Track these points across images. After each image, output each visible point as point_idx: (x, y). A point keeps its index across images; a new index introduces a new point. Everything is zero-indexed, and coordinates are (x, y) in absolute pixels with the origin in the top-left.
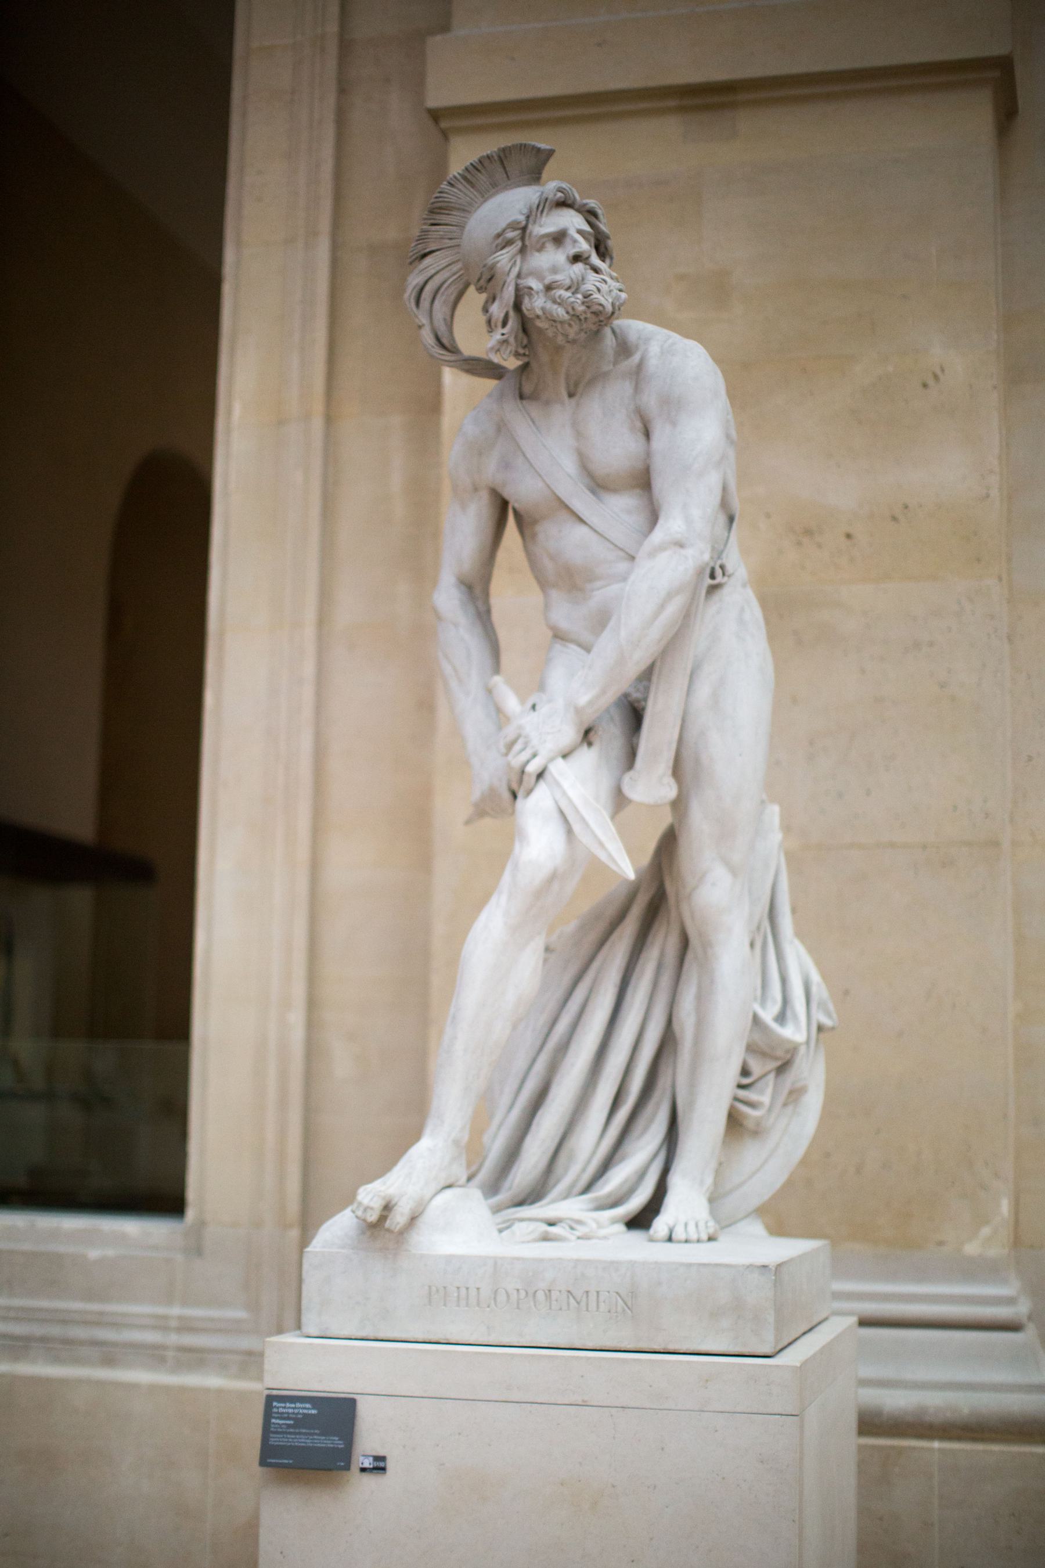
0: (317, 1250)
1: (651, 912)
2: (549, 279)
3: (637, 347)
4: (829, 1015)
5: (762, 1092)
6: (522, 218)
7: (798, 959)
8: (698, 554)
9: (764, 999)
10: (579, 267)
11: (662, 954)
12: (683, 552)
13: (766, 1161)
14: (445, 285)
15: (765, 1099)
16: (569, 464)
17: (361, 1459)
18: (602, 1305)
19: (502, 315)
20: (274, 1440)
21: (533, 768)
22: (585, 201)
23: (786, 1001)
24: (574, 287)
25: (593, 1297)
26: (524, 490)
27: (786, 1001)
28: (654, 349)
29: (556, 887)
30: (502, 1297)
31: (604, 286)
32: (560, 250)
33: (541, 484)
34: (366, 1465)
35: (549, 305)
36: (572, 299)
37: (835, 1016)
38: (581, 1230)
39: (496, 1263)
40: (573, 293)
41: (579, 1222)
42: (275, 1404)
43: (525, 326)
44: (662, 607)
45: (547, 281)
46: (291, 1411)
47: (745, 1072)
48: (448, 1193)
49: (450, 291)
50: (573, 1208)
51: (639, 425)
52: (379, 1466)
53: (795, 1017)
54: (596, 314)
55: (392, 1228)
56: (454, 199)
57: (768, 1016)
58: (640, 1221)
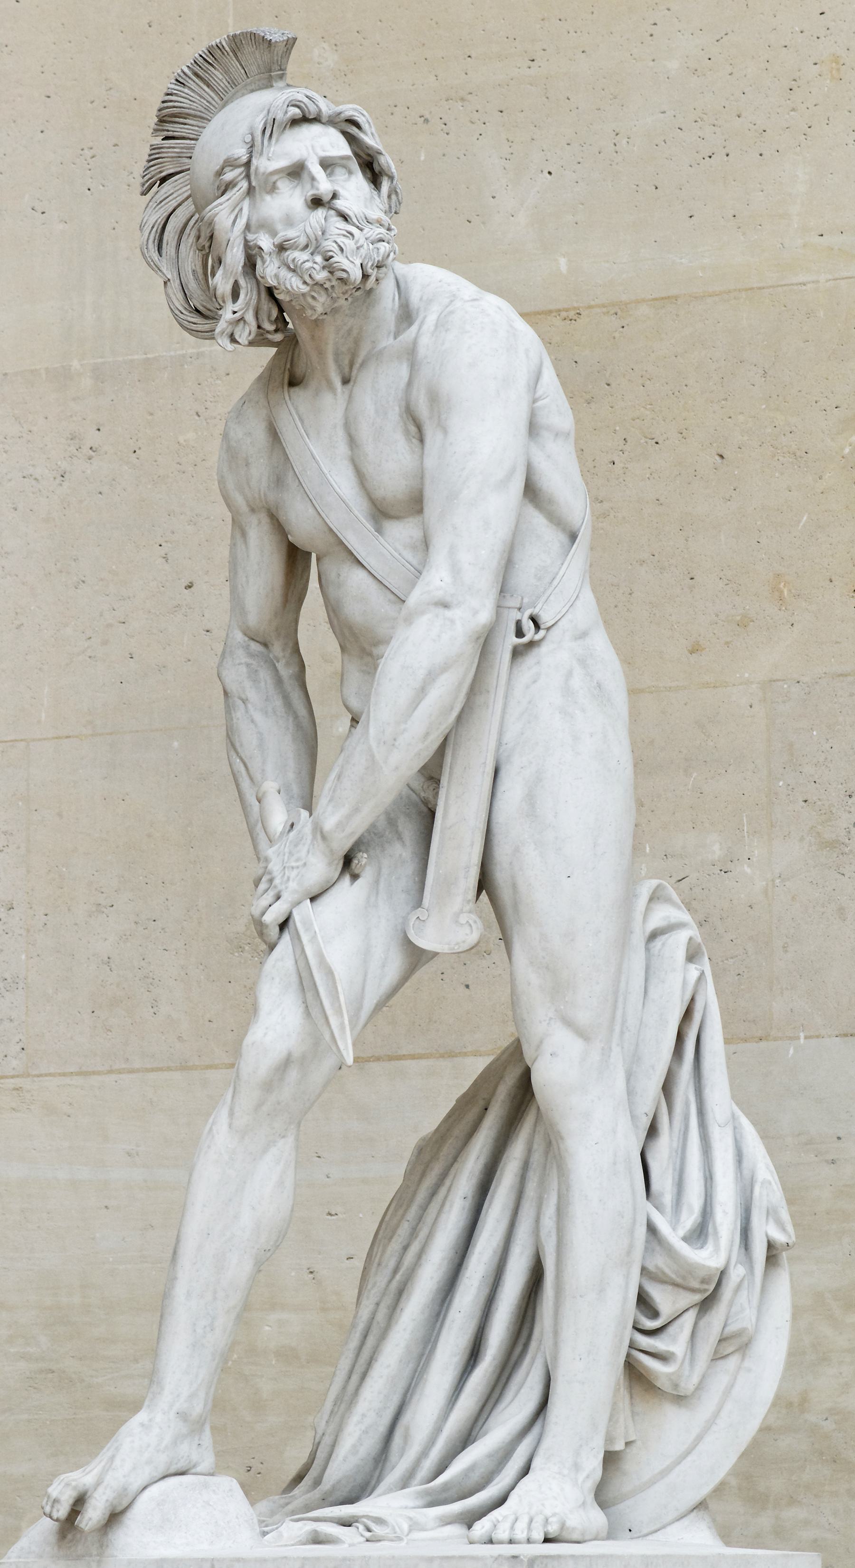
0: (11, 1560)
4: (783, 1229)
5: (674, 1340)
6: (241, 153)
11: (529, 1151)
12: (448, 613)
13: (699, 1438)
16: (344, 483)
19: (228, 288)
21: (272, 917)
22: (339, 109)
23: (707, 1213)
24: (313, 246)
27: (707, 1213)
29: (293, 1074)
33: (311, 510)
35: (284, 273)
36: (308, 265)
37: (790, 1228)
40: (312, 254)
44: (422, 691)
51: (413, 429)
56: (186, 103)
57: (673, 1235)
58: (470, 1519)
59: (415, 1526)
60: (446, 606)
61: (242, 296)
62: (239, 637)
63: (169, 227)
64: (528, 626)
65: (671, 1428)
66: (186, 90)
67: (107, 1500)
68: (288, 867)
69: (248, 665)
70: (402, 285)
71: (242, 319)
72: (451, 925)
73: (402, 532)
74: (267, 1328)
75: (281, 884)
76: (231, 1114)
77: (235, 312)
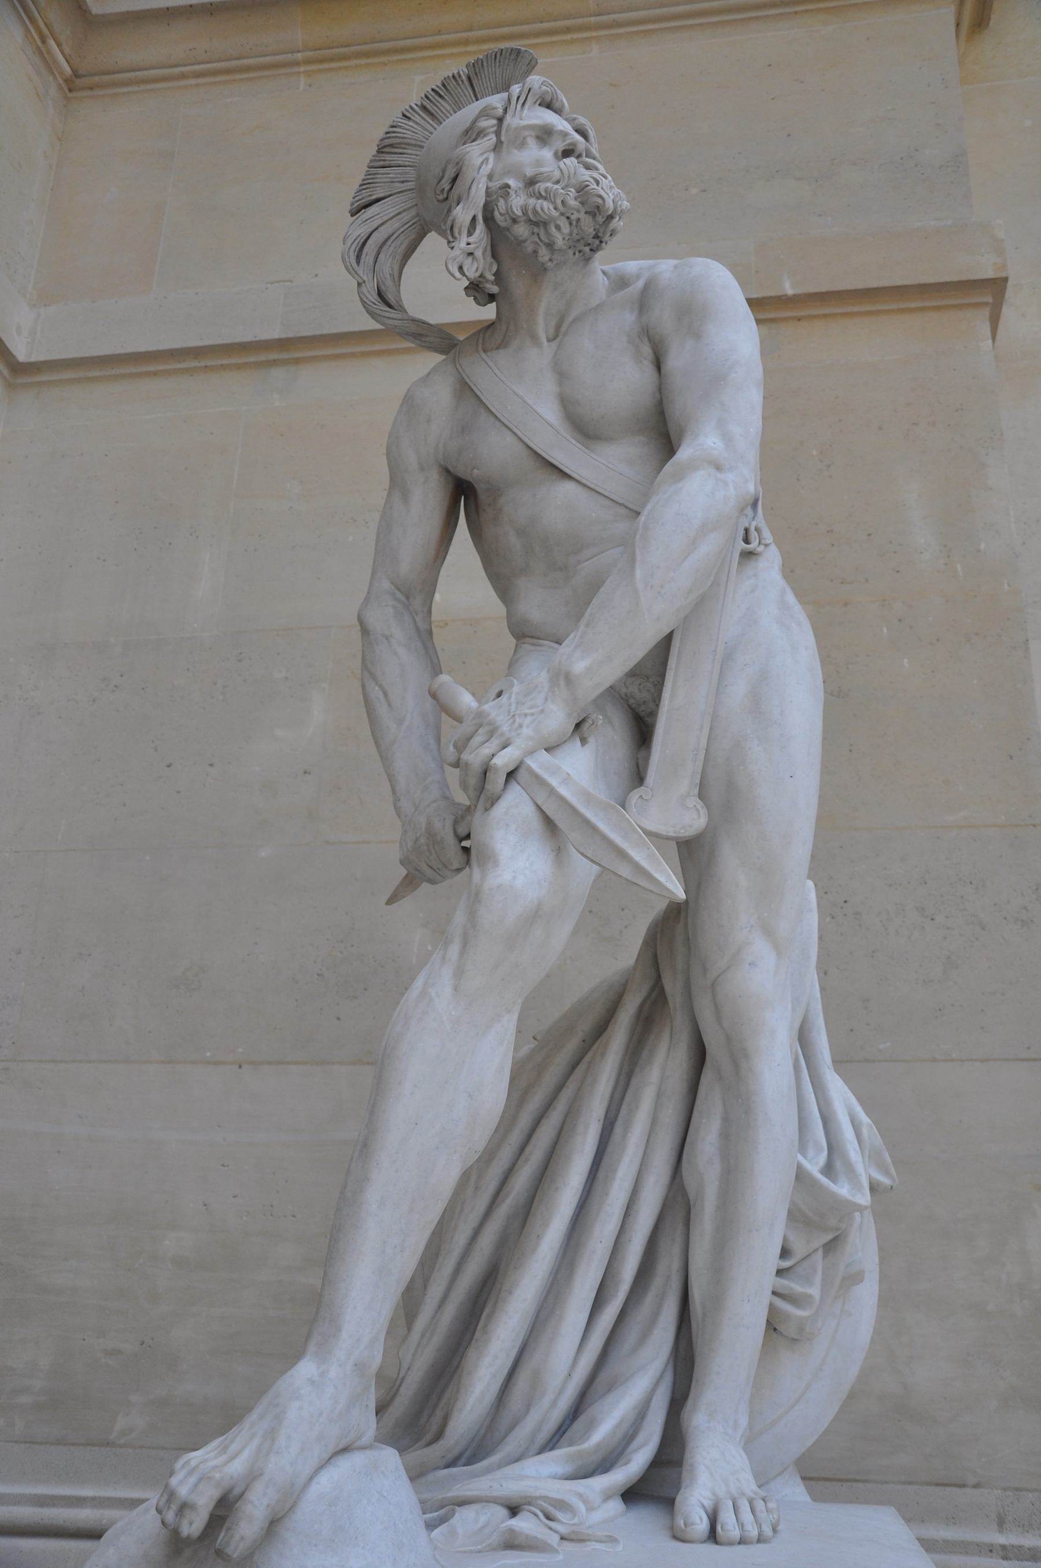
1: (653, 1005)
2: (529, 172)
4: (887, 1173)
5: (808, 1281)
7: (841, 1094)
9: (803, 1148)
10: (571, 161)
12: (719, 475)
14: (389, 243)
15: (815, 1291)
16: (550, 411)
21: (503, 760)
26: (493, 454)
33: (510, 438)
35: (532, 201)
37: (893, 1171)
38: (565, 1523)
41: (562, 1505)
47: (785, 1253)
48: (345, 1465)
49: (399, 241)
50: (540, 1475)
51: (647, 350)
55: (229, 1550)
57: (814, 1166)
62: (386, 585)
63: (370, 241)
66: (411, 123)
67: (268, 1506)
68: (519, 715)
69: (394, 607)
74: (167, 1242)
75: (510, 731)
76: (459, 973)
77: (468, 244)
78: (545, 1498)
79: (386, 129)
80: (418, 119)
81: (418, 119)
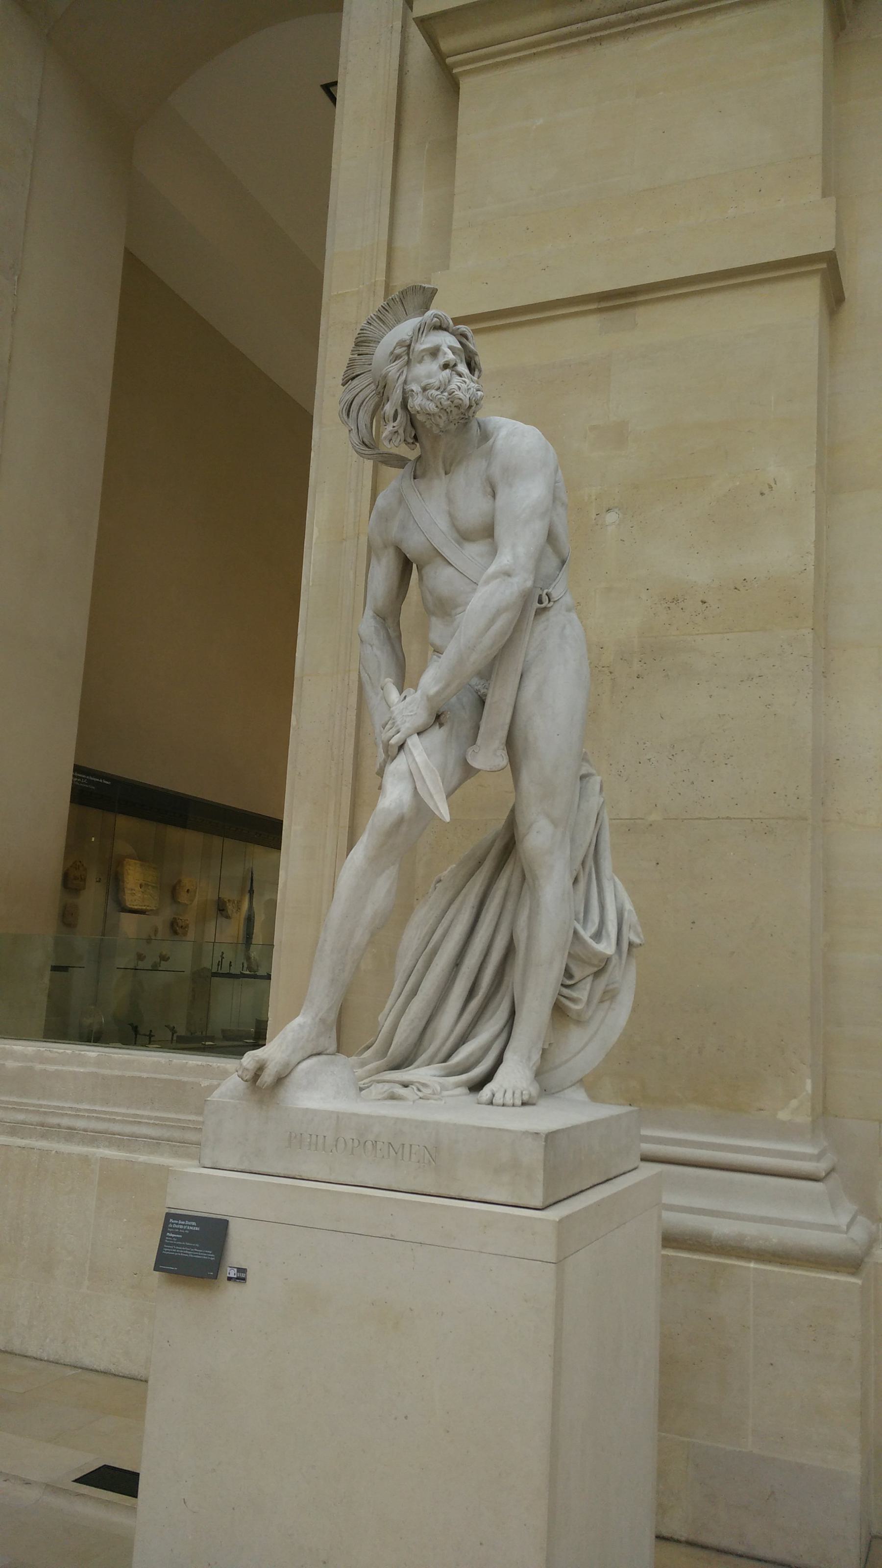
3: (493, 434)
4: (639, 937)
8: (522, 581)
12: (510, 579)
16: (443, 523)
17: (229, 1269)
18: (413, 1156)
19: (393, 412)
20: (166, 1251)
25: (407, 1149)
26: (413, 545)
28: (503, 433)
30: (341, 1145)
31: (463, 386)
32: (435, 362)
34: (232, 1275)
37: (642, 936)
39: (338, 1117)
41: (425, 1085)
42: (171, 1220)
43: (412, 421)
45: (423, 384)
46: (181, 1227)
48: (314, 1060)
51: (489, 490)
52: (241, 1277)
53: (608, 935)
54: (458, 407)
56: (371, 334)
57: (586, 935)
58: (477, 1086)
59: (444, 1088)
60: (509, 575)
61: (399, 419)
64: (545, 599)
65: (576, 1037)
70: (482, 425)
71: (396, 432)
72: (489, 756)
73: (475, 549)
78: (419, 1082)
79: (359, 331)
80: (375, 324)
81: (375, 324)
